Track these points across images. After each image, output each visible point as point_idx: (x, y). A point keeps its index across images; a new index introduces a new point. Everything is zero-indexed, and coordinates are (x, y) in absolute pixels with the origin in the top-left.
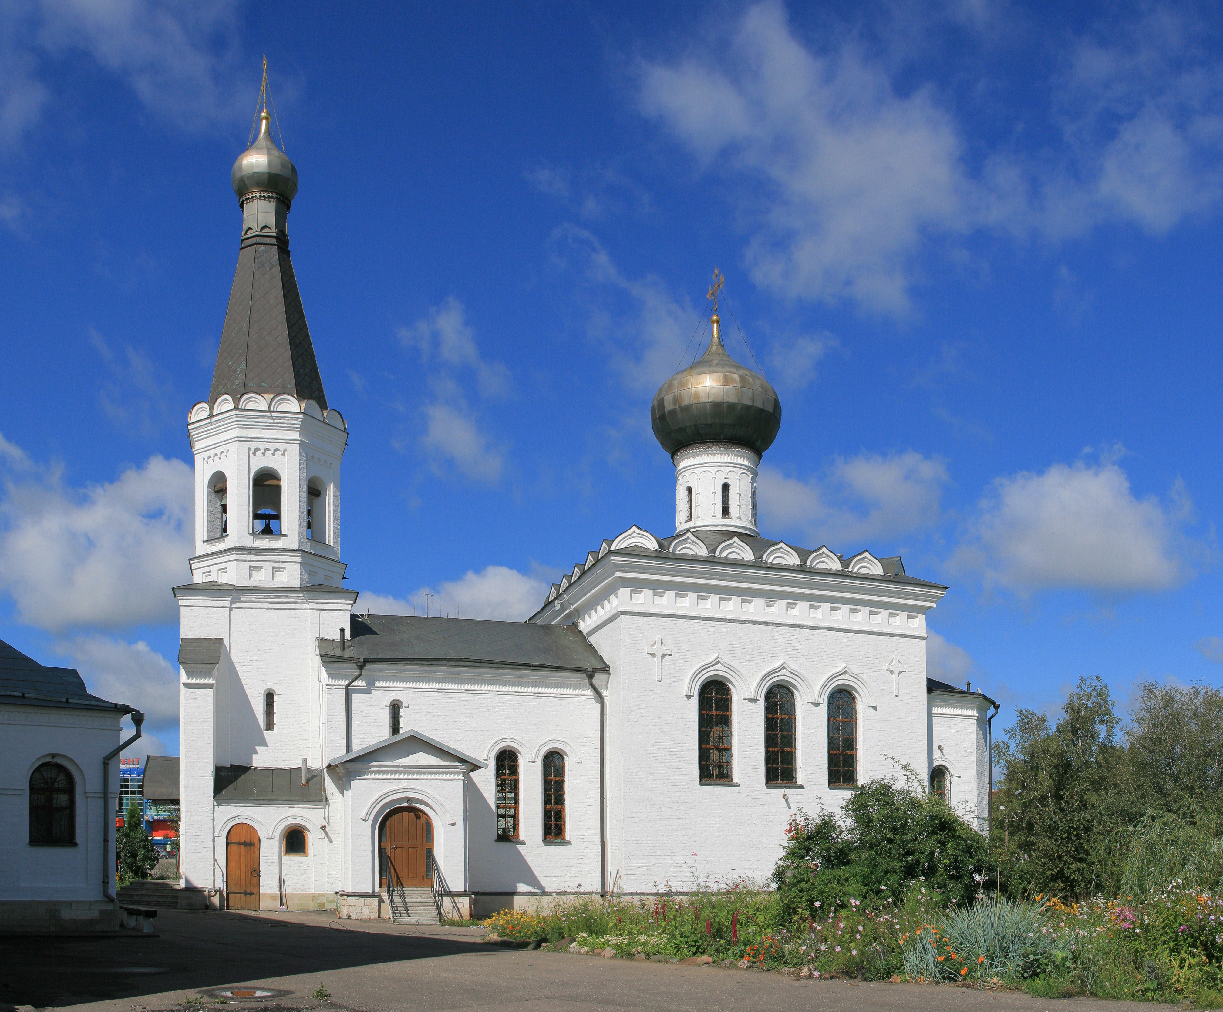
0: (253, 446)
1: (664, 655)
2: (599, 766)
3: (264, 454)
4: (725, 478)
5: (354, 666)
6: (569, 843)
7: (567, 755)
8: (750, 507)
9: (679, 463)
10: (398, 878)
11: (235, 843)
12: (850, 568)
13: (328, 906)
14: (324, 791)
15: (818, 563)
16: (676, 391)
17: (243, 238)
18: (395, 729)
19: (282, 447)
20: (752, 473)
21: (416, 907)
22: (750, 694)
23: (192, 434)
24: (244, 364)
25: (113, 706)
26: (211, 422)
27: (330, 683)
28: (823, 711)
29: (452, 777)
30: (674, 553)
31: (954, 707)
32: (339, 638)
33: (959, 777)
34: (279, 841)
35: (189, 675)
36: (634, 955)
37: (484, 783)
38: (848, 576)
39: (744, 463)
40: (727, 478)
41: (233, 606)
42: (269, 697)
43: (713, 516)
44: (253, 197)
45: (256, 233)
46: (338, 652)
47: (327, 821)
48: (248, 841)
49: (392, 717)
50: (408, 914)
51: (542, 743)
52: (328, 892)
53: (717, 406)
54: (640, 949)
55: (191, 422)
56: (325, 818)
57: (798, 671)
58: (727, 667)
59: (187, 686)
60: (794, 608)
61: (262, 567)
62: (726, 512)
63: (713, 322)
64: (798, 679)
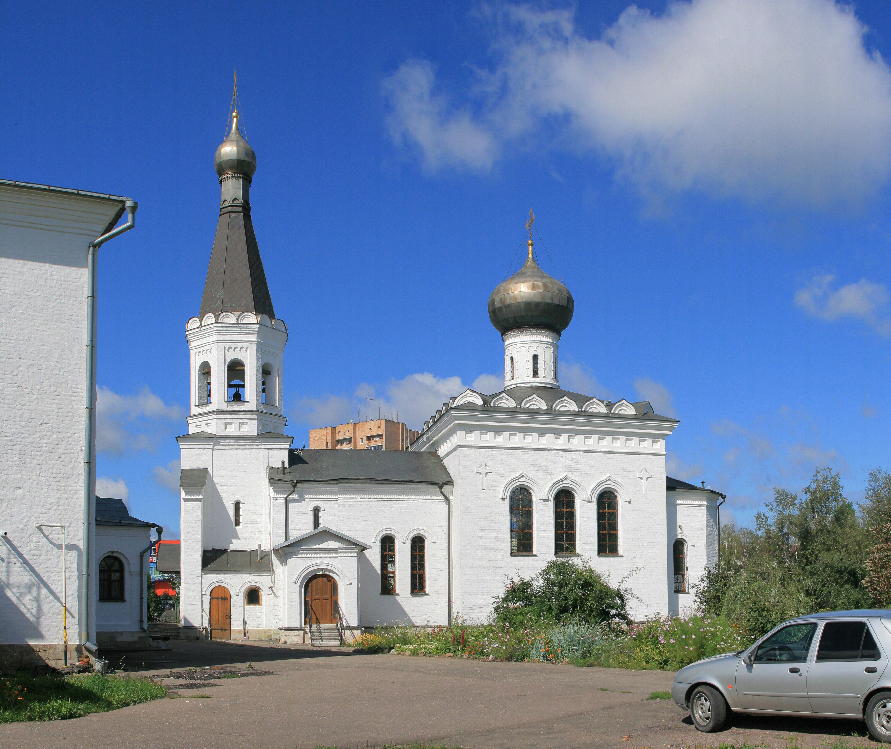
0: (228, 345)
1: (487, 473)
2: (447, 544)
3: (234, 350)
4: (535, 351)
5: (290, 485)
6: (427, 595)
7: (426, 538)
8: (552, 369)
9: (506, 341)
10: (317, 619)
11: (215, 598)
12: (613, 411)
13: (274, 637)
14: (272, 564)
15: (589, 409)
16: (502, 294)
17: (221, 207)
18: (316, 524)
19: (245, 345)
20: (553, 346)
21: (326, 636)
22: (544, 496)
23: (189, 337)
24: (222, 292)
25: (146, 524)
26: (201, 330)
27: (275, 496)
28: (594, 506)
29: (350, 555)
30: (494, 407)
31: (690, 499)
32: (281, 466)
33: (694, 546)
34: (243, 597)
35: (187, 493)
36: (419, 654)
37: (373, 557)
38: (609, 417)
39: (548, 340)
40: (536, 351)
41: (214, 448)
42: (237, 505)
43: (527, 376)
44: (227, 177)
45: (230, 204)
46: (281, 477)
47: (274, 583)
48: (223, 597)
49: (315, 517)
50: (321, 640)
51: (410, 531)
52: (274, 628)
53: (528, 305)
54: (422, 651)
55: (188, 329)
56: (272, 582)
57: (576, 480)
58: (529, 479)
59: (185, 500)
60: (574, 439)
61: (233, 423)
62: (535, 373)
63: (529, 245)
64: (576, 485)
